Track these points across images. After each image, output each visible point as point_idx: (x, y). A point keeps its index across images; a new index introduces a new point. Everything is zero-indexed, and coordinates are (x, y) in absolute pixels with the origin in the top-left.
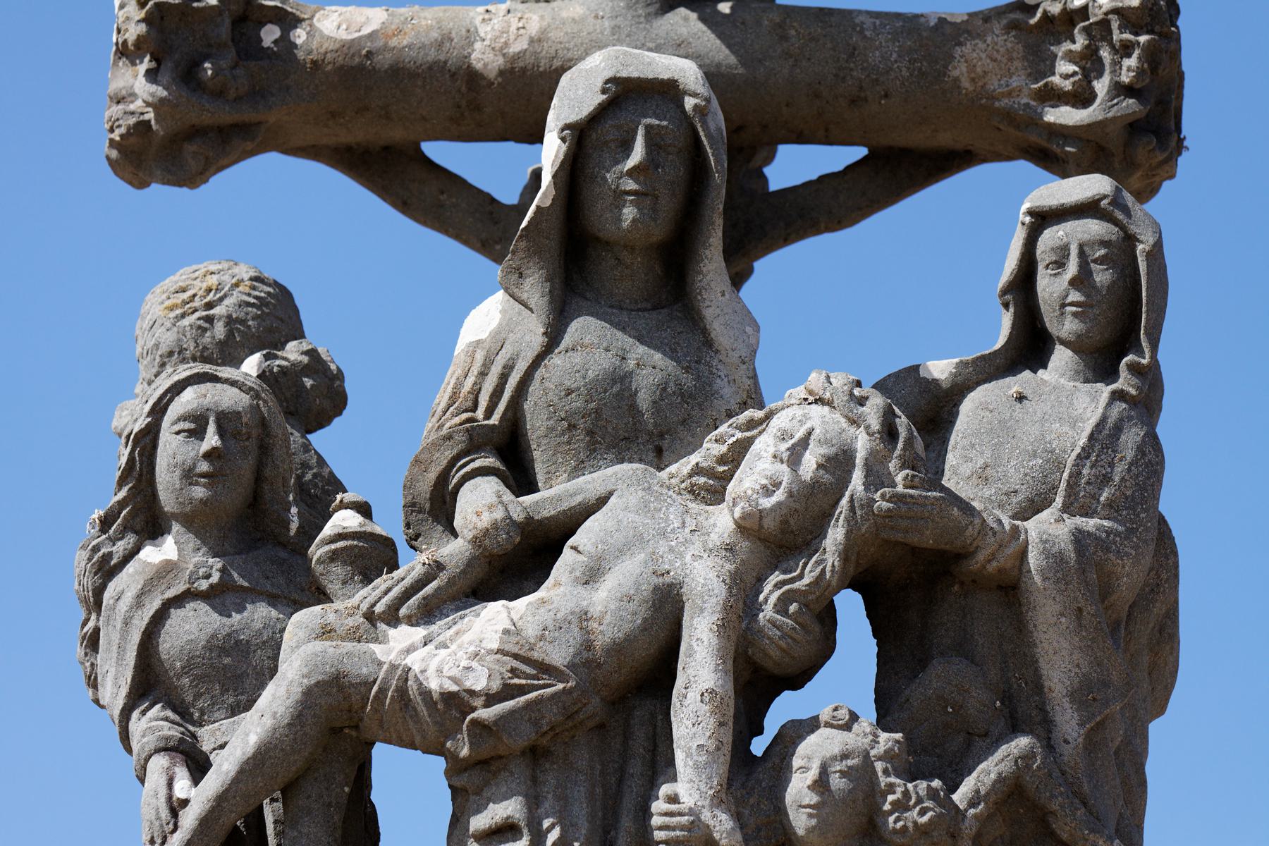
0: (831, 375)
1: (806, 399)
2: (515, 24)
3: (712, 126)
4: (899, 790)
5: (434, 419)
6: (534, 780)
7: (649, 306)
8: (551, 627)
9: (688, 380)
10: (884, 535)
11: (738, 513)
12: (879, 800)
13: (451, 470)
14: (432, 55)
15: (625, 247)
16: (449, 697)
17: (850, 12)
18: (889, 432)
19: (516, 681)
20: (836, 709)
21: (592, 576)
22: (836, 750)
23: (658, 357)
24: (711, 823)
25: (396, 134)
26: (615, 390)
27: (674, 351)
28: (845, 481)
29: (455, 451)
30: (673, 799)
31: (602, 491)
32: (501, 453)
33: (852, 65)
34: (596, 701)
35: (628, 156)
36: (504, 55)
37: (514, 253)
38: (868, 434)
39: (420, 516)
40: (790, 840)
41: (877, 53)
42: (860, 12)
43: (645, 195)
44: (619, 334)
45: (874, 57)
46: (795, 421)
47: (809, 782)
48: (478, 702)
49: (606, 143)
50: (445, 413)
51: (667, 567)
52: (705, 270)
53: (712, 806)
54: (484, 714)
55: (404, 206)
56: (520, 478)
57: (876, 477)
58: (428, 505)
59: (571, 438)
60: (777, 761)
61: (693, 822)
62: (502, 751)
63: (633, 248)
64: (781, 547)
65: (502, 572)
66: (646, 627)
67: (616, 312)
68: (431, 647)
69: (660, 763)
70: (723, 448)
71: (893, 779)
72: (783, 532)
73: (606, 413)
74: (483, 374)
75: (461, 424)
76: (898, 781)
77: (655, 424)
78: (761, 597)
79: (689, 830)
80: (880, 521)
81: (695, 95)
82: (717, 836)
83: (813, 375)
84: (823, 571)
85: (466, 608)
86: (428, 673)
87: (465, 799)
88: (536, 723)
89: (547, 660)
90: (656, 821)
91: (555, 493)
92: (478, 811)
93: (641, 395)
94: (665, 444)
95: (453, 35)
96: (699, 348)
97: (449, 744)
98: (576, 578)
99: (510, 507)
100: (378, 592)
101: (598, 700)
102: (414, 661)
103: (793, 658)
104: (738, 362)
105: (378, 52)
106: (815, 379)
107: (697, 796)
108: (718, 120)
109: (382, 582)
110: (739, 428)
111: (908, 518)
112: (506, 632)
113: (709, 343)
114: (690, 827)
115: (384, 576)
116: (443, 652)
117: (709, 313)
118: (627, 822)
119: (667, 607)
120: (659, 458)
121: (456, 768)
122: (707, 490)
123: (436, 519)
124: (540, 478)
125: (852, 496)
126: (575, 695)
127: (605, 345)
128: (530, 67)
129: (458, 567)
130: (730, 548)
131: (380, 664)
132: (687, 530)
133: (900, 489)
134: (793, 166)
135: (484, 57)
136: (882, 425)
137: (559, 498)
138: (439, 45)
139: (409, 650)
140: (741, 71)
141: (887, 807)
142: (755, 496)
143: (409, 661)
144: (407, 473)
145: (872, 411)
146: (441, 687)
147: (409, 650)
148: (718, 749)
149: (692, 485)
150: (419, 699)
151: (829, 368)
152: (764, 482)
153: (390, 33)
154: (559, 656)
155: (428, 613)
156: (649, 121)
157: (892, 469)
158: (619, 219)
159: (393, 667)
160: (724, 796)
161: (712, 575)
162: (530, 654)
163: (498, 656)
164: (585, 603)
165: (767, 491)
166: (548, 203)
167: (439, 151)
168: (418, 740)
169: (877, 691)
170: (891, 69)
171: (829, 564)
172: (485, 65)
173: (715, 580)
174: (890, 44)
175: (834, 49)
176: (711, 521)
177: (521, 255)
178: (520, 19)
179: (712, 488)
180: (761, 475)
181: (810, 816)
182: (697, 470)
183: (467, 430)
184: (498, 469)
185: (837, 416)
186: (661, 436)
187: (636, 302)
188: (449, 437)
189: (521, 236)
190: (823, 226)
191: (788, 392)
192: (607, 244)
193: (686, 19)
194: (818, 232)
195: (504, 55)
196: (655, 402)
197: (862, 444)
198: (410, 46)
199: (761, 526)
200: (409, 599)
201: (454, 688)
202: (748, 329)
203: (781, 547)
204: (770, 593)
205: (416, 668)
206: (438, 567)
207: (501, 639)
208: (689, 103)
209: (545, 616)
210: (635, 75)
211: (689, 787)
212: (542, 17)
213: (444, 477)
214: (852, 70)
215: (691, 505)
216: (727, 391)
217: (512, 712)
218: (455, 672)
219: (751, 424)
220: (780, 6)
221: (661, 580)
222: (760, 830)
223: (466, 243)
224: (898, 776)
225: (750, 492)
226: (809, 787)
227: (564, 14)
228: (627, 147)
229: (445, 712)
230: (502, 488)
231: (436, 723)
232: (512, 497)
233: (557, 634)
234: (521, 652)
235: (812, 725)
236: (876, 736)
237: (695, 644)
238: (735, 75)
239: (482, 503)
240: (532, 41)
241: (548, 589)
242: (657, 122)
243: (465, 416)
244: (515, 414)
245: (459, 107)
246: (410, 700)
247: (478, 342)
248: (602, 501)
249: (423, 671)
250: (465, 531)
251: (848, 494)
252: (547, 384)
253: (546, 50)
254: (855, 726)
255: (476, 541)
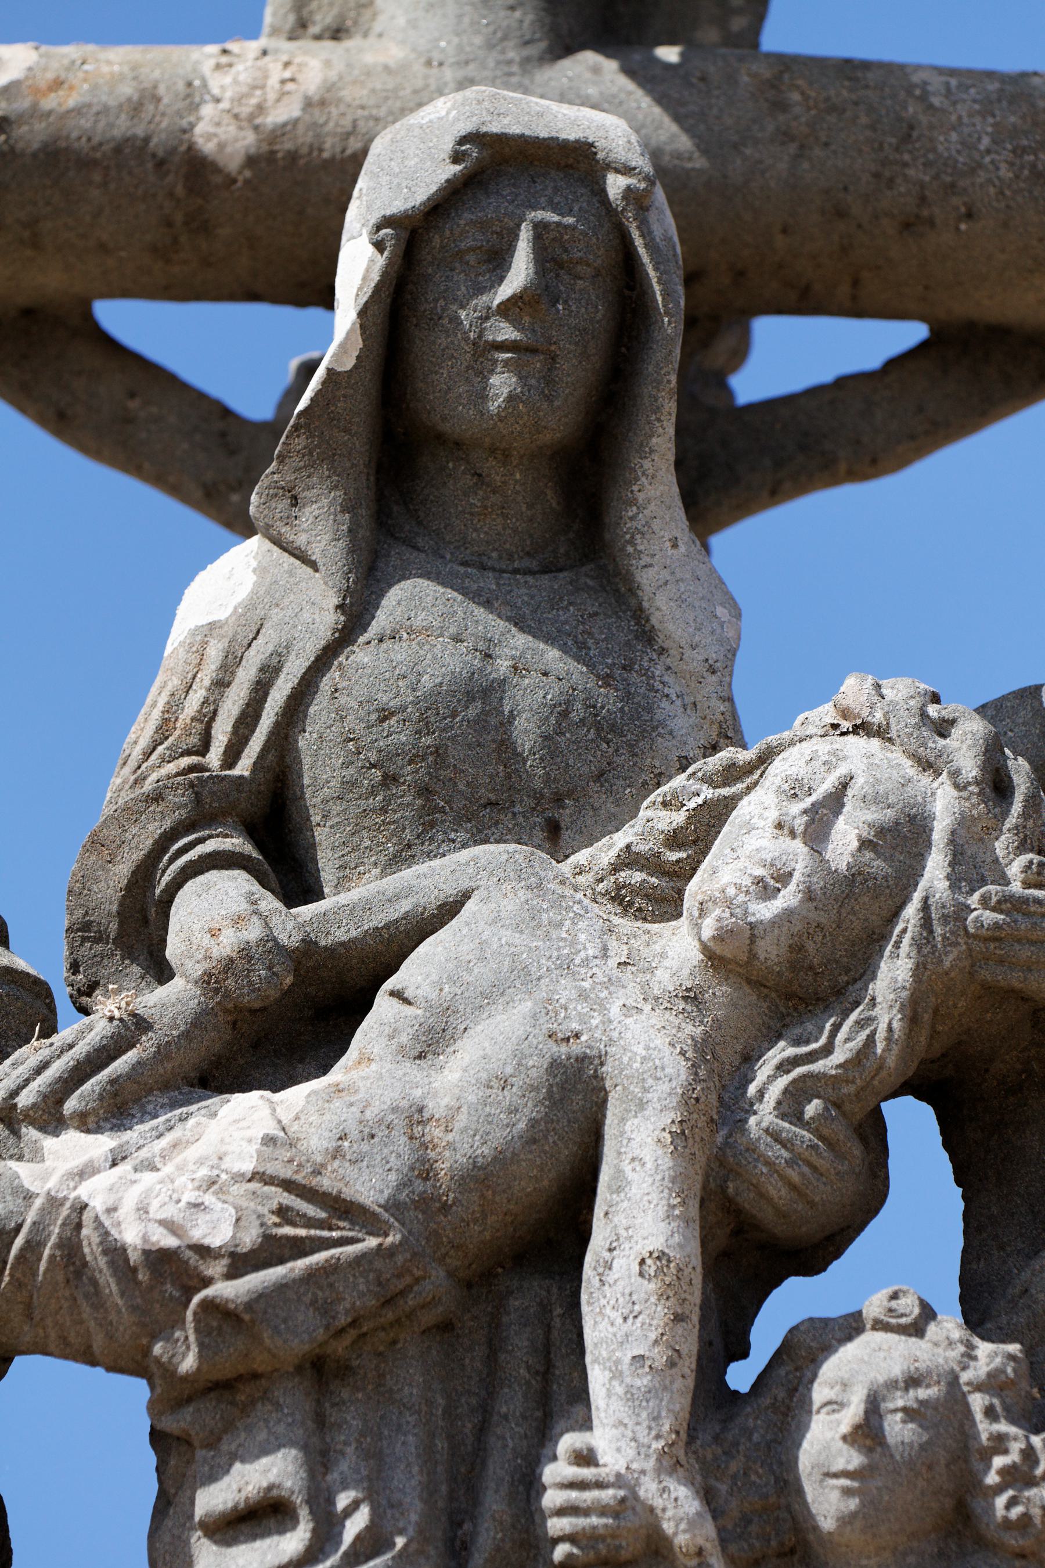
0: (883, 682)
1: (835, 726)
2: (276, 73)
3: (657, 232)
4: (1016, 1448)
5: (127, 770)
6: (321, 1421)
7: (534, 565)
8: (354, 1134)
9: (609, 700)
10: (985, 974)
11: (708, 928)
12: (977, 1466)
13: (159, 859)
14: (123, 126)
15: (492, 450)
16: (161, 1260)
17: (902, 67)
18: (997, 785)
19: (288, 1230)
20: (895, 1296)
21: (431, 1043)
22: (897, 1370)
23: (553, 654)
24: (658, 1503)
25: (48, 280)
26: (472, 712)
27: (582, 646)
28: (910, 875)
29: (168, 824)
30: (586, 1458)
31: (450, 890)
32: (251, 831)
33: (907, 157)
34: (438, 1274)
35: (501, 279)
36: (256, 128)
37: (282, 459)
38: (957, 786)
39: (99, 948)
40: (805, 1544)
41: (954, 136)
42: (918, 67)
43: (532, 350)
44: (480, 612)
45: (948, 143)
46: (816, 764)
47: (845, 1428)
48: (215, 1268)
49: (460, 254)
50: (147, 755)
51: (575, 1026)
52: (641, 497)
53: (659, 1471)
54: (228, 1290)
55: (60, 422)
56: (290, 872)
57: (970, 867)
58: (114, 926)
59: (388, 801)
60: (781, 1395)
61: (623, 1500)
62: (260, 1362)
63: (506, 455)
64: (789, 997)
65: (256, 1046)
66: (533, 1138)
67: (471, 570)
68: (124, 1168)
69: (559, 1392)
70: (679, 818)
71: (1003, 1427)
72: (794, 966)
73: (455, 753)
74: (221, 684)
75: (178, 774)
76: (1012, 1430)
77: (547, 780)
78: (752, 1090)
79: (616, 1515)
80: (978, 946)
81: (627, 170)
82: (668, 1527)
83: (850, 683)
84: (871, 1040)
85: (189, 1102)
86: (121, 1214)
87: (179, 1455)
88: (325, 1309)
89: (348, 1194)
90: (552, 1498)
91: (353, 900)
92: (212, 1478)
93: (521, 723)
94: (565, 816)
95: (162, 90)
96: (628, 643)
97: (158, 1349)
98: (401, 1050)
99: (274, 921)
100: (23, 1070)
101: (442, 1274)
102: (94, 1193)
103: (812, 1204)
104: (703, 669)
105: (22, 118)
106: (854, 690)
107: (631, 1453)
108: (665, 222)
109: (29, 1055)
110: (708, 780)
111: (1032, 943)
112: (269, 1141)
113: (646, 635)
114: (618, 1510)
115: (34, 1043)
116: (148, 1178)
117: (647, 579)
118: (494, 1503)
119: (574, 1101)
120: (555, 839)
121: (172, 1395)
122: (647, 896)
123: (129, 954)
124: (328, 876)
125: (926, 900)
126: (400, 1259)
127: (453, 630)
128: (304, 150)
129: (176, 1026)
130: (692, 997)
131: (29, 1197)
132: (612, 962)
133: (1016, 887)
134: (789, 356)
135: (220, 131)
136: (983, 769)
137: (367, 906)
138: (136, 108)
139: (83, 1173)
140: (700, 162)
141: (992, 1478)
142: (742, 898)
143: (83, 1191)
144: (74, 866)
145: (965, 747)
146: (145, 1239)
147: (83, 1173)
148: (671, 1364)
149: (619, 887)
150: (102, 1261)
151: (880, 670)
152: (759, 872)
153: (43, 85)
154: (369, 1186)
155: (118, 1110)
156: (540, 215)
157: (1000, 852)
158: (482, 395)
159: (54, 1202)
160: (681, 1454)
161: (660, 1041)
162: (315, 1181)
163: (254, 1185)
164: (418, 1093)
165: (765, 890)
166: (349, 363)
167: (123, 318)
168: (98, 1342)
169: (964, 1280)
170: (980, 166)
171: (882, 1027)
172: (222, 146)
173: (667, 1050)
174: (977, 120)
175: (873, 127)
176: (657, 948)
177: (295, 461)
178: (287, 64)
179: (656, 890)
180: (754, 860)
181: (847, 1492)
182: (629, 859)
183: (192, 785)
184: (250, 857)
185: (897, 755)
186: (558, 800)
187: (511, 557)
188: (156, 797)
189: (296, 427)
190: (843, 467)
191: (801, 718)
192: (458, 446)
193: (596, 70)
194: (835, 481)
195: (256, 128)
196: (546, 738)
197: (944, 805)
198: (79, 111)
199: (752, 955)
200: (82, 1082)
201: (170, 1242)
202: (720, 611)
203: (789, 997)
204: (769, 1081)
205: (98, 1204)
206: (139, 1024)
207: (259, 1153)
208: (616, 185)
209: (343, 1114)
210: (516, 130)
211: (617, 1436)
212: (328, 63)
213: (145, 872)
214: (905, 165)
215: (616, 920)
216: (681, 723)
217: (281, 1288)
218: (170, 1212)
219: (732, 773)
220: (768, 55)
221: (564, 1048)
222: (749, 1522)
223: (175, 490)
224: (1013, 1421)
225: (731, 891)
226: (844, 1438)
227: (369, 58)
228: (498, 261)
229: (151, 1288)
230: (256, 887)
231: (134, 1309)
232: (278, 905)
233: (365, 1147)
234: (299, 1178)
235: (851, 1326)
236: (970, 1346)
237: (627, 1168)
238: (688, 172)
239: (217, 915)
240: (308, 104)
241: (347, 1070)
242: (556, 218)
243: (186, 761)
244: (282, 757)
245: (169, 224)
246: (85, 1264)
247: (212, 626)
248: (449, 910)
249: (111, 1210)
250: (189, 964)
251: (917, 896)
252: (343, 700)
253: (336, 120)
254: (932, 1329)
255: (210, 982)
